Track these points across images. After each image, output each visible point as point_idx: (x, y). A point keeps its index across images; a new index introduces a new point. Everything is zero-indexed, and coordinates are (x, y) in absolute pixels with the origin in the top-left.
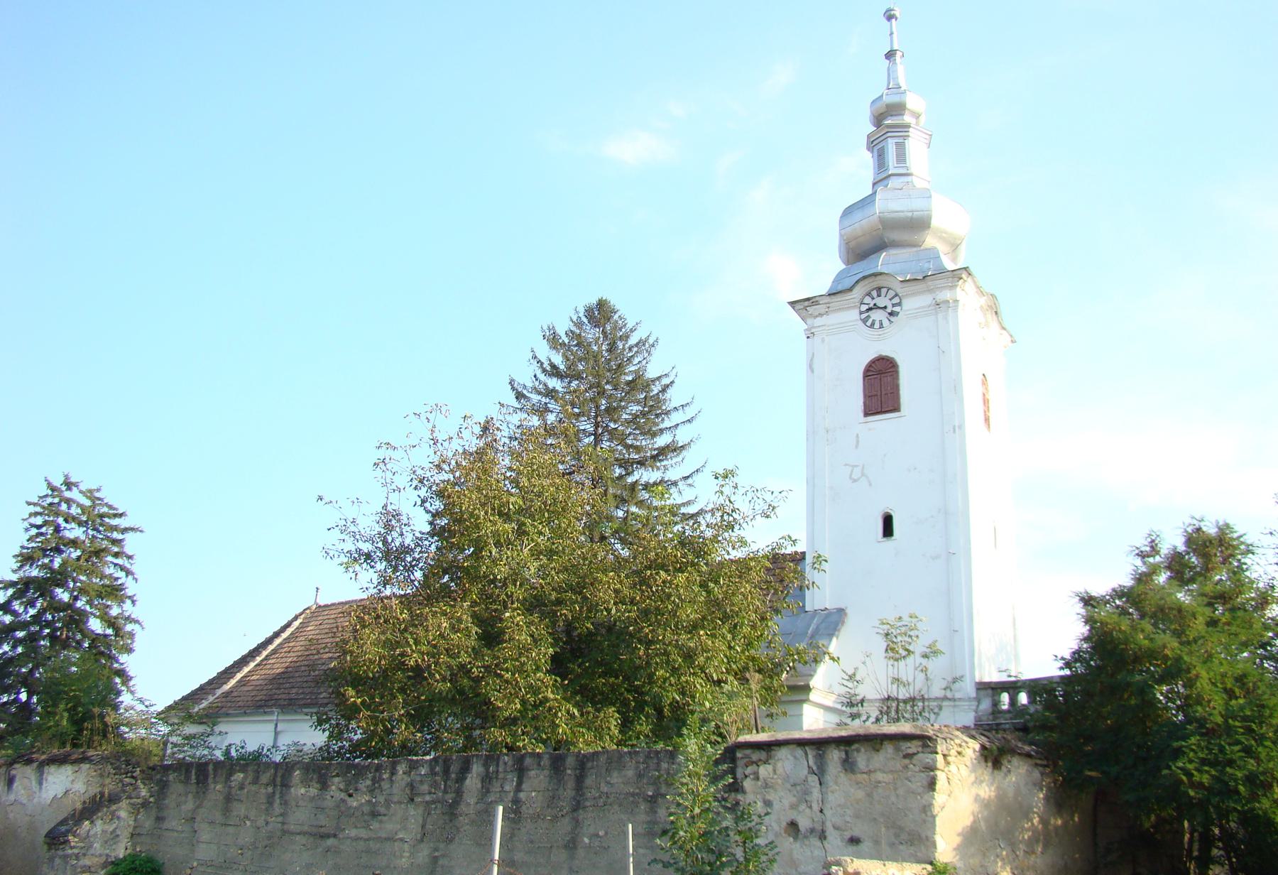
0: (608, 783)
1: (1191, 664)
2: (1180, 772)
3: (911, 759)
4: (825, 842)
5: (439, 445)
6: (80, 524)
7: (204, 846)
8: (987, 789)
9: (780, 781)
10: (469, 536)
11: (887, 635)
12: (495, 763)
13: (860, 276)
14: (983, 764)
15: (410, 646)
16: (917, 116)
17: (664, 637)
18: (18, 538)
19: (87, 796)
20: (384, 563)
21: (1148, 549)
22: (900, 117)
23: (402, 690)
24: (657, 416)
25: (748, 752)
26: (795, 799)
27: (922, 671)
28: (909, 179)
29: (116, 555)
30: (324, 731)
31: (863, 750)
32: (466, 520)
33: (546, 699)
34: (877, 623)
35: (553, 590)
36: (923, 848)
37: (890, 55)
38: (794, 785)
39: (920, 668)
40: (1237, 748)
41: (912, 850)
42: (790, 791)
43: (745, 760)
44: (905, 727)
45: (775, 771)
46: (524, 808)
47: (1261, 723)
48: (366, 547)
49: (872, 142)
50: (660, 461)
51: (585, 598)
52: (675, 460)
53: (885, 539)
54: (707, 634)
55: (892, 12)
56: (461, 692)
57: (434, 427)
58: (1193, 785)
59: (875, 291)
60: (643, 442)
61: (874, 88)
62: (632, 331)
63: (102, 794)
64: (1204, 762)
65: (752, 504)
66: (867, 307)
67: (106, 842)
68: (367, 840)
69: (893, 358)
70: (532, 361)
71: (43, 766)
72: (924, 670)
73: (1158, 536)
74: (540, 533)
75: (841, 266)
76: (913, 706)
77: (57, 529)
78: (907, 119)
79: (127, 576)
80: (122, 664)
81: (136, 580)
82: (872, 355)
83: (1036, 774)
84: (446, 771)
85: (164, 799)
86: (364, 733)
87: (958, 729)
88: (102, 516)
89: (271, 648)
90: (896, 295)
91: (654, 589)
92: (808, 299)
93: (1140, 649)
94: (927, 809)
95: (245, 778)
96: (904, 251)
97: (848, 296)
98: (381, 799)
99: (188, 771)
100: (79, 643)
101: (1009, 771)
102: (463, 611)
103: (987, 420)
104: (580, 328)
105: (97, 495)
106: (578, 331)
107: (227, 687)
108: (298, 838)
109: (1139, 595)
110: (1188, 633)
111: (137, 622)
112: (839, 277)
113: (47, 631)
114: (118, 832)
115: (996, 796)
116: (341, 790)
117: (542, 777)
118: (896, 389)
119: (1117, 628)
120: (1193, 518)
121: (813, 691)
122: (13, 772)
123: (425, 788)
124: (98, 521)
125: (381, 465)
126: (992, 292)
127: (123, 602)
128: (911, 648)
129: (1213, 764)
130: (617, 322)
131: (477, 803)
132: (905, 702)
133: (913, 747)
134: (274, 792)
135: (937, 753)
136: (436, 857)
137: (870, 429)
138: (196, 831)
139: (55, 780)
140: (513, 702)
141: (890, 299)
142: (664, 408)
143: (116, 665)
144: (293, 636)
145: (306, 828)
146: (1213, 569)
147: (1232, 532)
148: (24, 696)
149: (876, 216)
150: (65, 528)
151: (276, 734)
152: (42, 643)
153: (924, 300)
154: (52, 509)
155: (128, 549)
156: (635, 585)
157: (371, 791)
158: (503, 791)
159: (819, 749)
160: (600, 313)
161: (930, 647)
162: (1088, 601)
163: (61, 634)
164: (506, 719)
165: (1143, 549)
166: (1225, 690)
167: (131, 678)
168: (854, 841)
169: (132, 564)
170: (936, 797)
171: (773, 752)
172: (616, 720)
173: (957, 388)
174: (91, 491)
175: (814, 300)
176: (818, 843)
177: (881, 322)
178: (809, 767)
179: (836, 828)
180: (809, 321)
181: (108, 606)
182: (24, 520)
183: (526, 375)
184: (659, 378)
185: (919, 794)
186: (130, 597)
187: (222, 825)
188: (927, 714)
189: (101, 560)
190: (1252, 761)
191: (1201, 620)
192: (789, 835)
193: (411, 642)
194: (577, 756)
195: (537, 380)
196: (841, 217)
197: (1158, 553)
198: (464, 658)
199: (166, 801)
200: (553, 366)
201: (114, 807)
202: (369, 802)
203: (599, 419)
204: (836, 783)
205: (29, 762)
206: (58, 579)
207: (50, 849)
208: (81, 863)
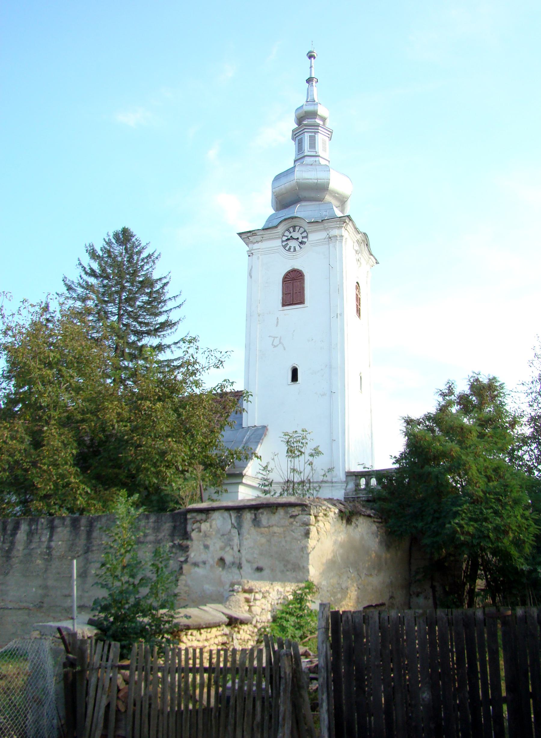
1: (466, 461)
2: (455, 525)
4: (241, 571)
5: (5, 319)
10: (24, 377)
11: (288, 442)
12: (35, 523)
13: (283, 218)
14: (340, 521)
16: (324, 119)
21: (447, 391)
25: (194, 514)
27: (309, 464)
28: (317, 159)
31: (265, 513)
32: (41, 407)
35: (79, 412)
36: (301, 573)
38: (223, 535)
39: (308, 462)
40: (490, 511)
41: (294, 574)
42: (220, 539)
43: (192, 520)
44: (292, 499)
45: (211, 526)
47: (505, 496)
49: (295, 135)
52: (170, 331)
53: (292, 383)
54: (173, 441)
55: (312, 54)
56: (16, 477)
58: (463, 533)
59: (292, 228)
60: (148, 319)
61: (300, 100)
62: (143, 248)
64: (471, 519)
65: (208, 359)
66: (286, 238)
70: (78, 266)
72: (311, 464)
73: (453, 383)
78: (318, 121)
82: (289, 268)
83: (374, 527)
90: (305, 231)
91: (143, 413)
92: (250, 232)
93: (437, 451)
94: (304, 549)
97: (275, 231)
102: (19, 425)
103: (358, 311)
104: (110, 246)
106: (109, 248)
109: (440, 419)
110: (466, 442)
117: (65, 532)
118: (303, 289)
119: (424, 438)
120: (473, 372)
121: (245, 477)
126: (364, 232)
128: (303, 450)
129: (476, 521)
130: (134, 243)
131: (24, 549)
132: (299, 483)
133: (295, 511)
135: (310, 515)
137: (285, 315)
140: (48, 484)
141: (301, 234)
142: (162, 299)
146: (484, 403)
147: (496, 382)
149: (294, 181)
153: (322, 235)
158: (40, 541)
159: (238, 512)
161: (315, 449)
162: (409, 422)
165: (444, 391)
166: (486, 476)
168: (259, 569)
170: (309, 542)
171: (210, 515)
173: (340, 290)
175: (253, 232)
177: (295, 247)
178: (232, 524)
179: (248, 561)
180: (250, 245)
184: (160, 279)
185: (299, 540)
188: (312, 491)
190: (498, 518)
191: (475, 434)
192: (219, 566)
194: (88, 519)
195: (81, 279)
196: (273, 181)
197: (453, 394)
198: (18, 456)
200: (92, 270)
204: (249, 534)
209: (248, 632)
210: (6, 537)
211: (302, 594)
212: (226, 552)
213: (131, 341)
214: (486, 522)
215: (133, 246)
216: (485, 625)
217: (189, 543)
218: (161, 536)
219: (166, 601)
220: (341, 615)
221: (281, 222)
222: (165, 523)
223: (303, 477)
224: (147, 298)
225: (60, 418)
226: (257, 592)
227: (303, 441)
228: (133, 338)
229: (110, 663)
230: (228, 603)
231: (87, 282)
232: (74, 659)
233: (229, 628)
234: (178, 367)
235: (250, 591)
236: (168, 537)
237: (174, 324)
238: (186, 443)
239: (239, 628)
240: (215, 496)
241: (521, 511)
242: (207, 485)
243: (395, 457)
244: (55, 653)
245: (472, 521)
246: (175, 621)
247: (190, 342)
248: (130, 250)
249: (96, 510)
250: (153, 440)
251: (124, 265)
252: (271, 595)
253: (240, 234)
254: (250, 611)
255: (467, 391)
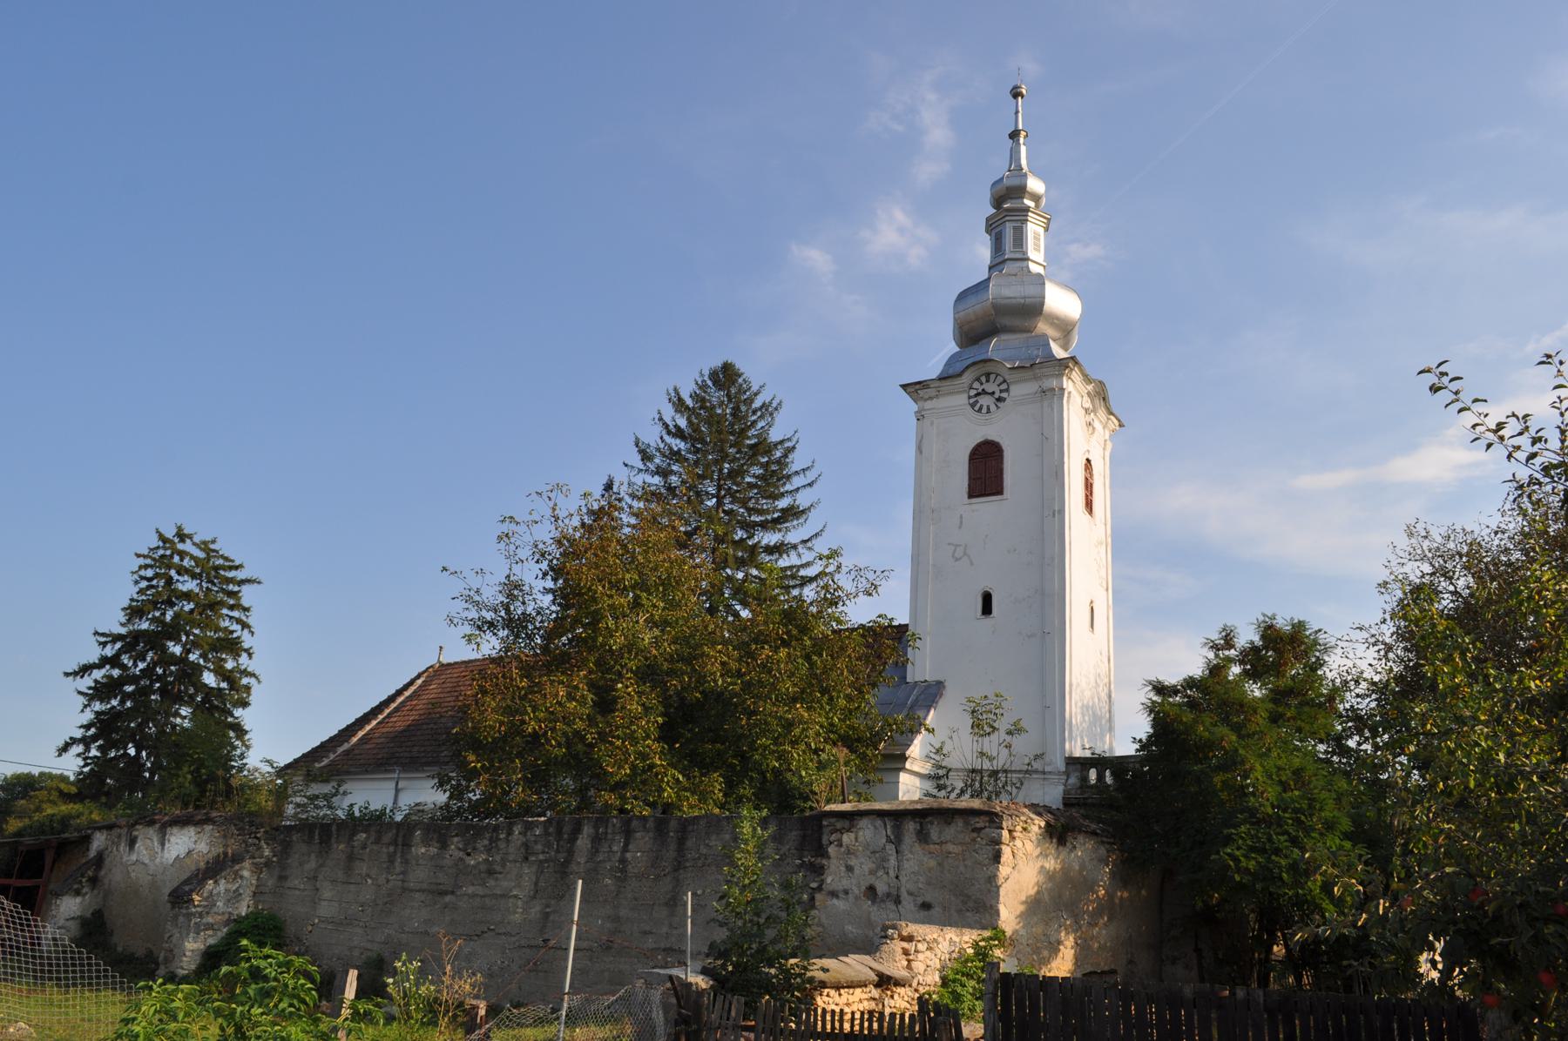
0: (708, 845)
3: (979, 833)
4: (900, 907)
6: (194, 576)
7: (323, 903)
8: (1052, 861)
9: (860, 848)
11: (973, 712)
14: (1048, 839)
15: (529, 715)
17: (764, 709)
18: (127, 591)
19: (210, 856)
20: (506, 632)
21: (1222, 642)
22: (1019, 201)
23: (519, 755)
24: (779, 480)
25: (833, 820)
26: (874, 865)
29: (232, 608)
30: (445, 791)
32: (584, 594)
33: (652, 766)
34: (964, 701)
36: (987, 915)
37: (1014, 135)
40: (1282, 838)
41: (977, 917)
44: (976, 804)
45: (856, 839)
46: (630, 867)
48: (489, 616)
50: (781, 523)
51: (694, 670)
52: (795, 522)
57: (556, 505)
58: (1238, 870)
60: (764, 504)
61: (998, 168)
62: (756, 394)
63: (226, 854)
64: (1252, 849)
66: (975, 392)
67: (229, 901)
68: (482, 897)
69: (998, 443)
71: (166, 828)
72: (1009, 746)
73: (1232, 631)
74: (654, 606)
75: (953, 348)
76: (996, 780)
77: (169, 581)
78: (1028, 202)
79: (242, 630)
80: (237, 718)
81: (253, 633)
83: (1103, 851)
84: (559, 832)
85: (287, 859)
86: (484, 794)
87: (1026, 807)
88: (216, 568)
89: (393, 706)
90: (1005, 381)
92: (919, 383)
95: (367, 838)
96: (1018, 336)
97: (957, 381)
98: (498, 858)
99: (311, 833)
100: (192, 697)
101: (1075, 847)
104: (705, 392)
105: (212, 546)
107: (346, 746)
108: (417, 895)
111: (253, 675)
112: (952, 360)
113: (158, 685)
114: (241, 891)
115: (1062, 869)
116: (460, 849)
120: (1264, 615)
122: (135, 833)
123: (539, 847)
124: (213, 573)
125: (505, 539)
126: (1100, 379)
127: (239, 656)
128: (996, 725)
129: (1262, 851)
131: (586, 862)
133: (980, 822)
134: (395, 852)
136: (548, 913)
137: (973, 511)
138: (317, 889)
139: (178, 841)
140: (623, 768)
143: (230, 719)
144: (415, 695)
145: (425, 886)
148: (132, 752)
150: (178, 581)
151: (397, 791)
152: (153, 697)
154: (164, 562)
155: (245, 602)
156: (741, 657)
157: (489, 850)
160: (726, 376)
161: (1014, 724)
162: (1160, 688)
163: (173, 688)
164: (617, 783)
167: (246, 732)
168: (926, 906)
169: (247, 617)
171: (855, 822)
172: (720, 784)
173: (1057, 474)
174: (205, 543)
176: (894, 908)
179: (910, 894)
180: (920, 403)
181: (223, 660)
182: (133, 573)
183: (652, 436)
184: (782, 442)
186: (247, 651)
187: (344, 883)
188: (1009, 788)
189: (216, 613)
190: (1296, 850)
192: (868, 899)
193: (529, 709)
198: (579, 725)
199: (289, 861)
201: (237, 867)
202: (486, 860)
203: (722, 482)
204: (911, 852)
205: (151, 823)
206: (171, 631)
207: (173, 908)
208: (204, 920)
209: (906, 999)
210: (561, 843)
211: (985, 947)
212: (877, 878)
213: (737, 538)
214: (1277, 855)
215: (741, 391)
216: (1195, 1007)
217: (824, 862)
218: (784, 849)
219: (798, 948)
220: (1013, 979)
221: (967, 368)
222: (791, 830)
223: (998, 764)
224: (761, 471)
225: (638, 668)
226: (919, 941)
227: (997, 711)
228: (740, 534)
229: (731, 1022)
230: (878, 954)
231: (671, 449)
232: (688, 1016)
233: (879, 990)
234: (811, 580)
235: (910, 939)
236: (794, 852)
237: (803, 512)
238: (822, 708)
239: (892, 992)
240: (862, 789)
241: (1338, 841)
242: (851, 772)
243: (1140, 741)
244: (666, 1007)
245: (1254, 852)
246: (809, 974)
247: (828, 558)
248: (735, 397)
249: (691, 807)
250: (774, 704)
251: (727, 420)
252: (940, 946)
253: (904, 387)
254: (909, 967)
255: (1257, 639)
